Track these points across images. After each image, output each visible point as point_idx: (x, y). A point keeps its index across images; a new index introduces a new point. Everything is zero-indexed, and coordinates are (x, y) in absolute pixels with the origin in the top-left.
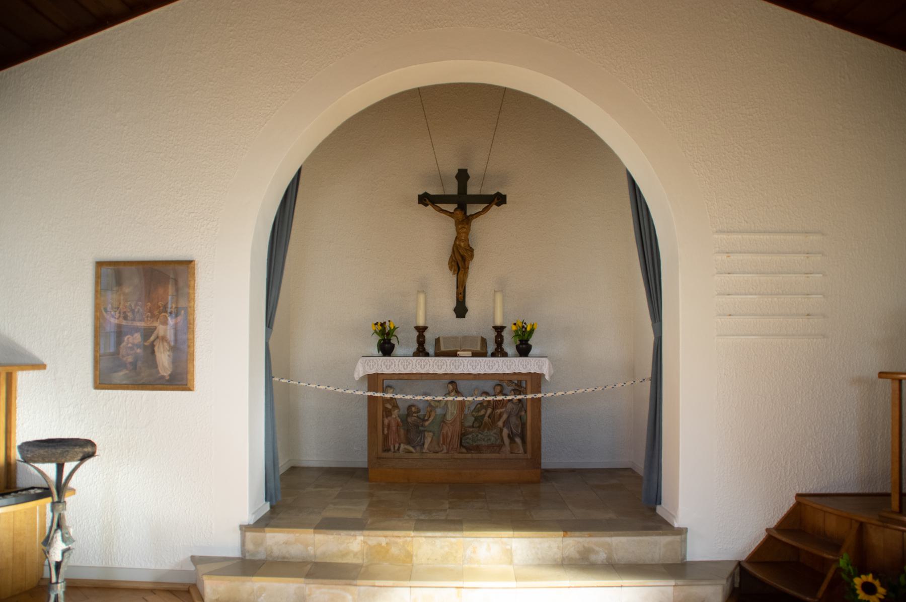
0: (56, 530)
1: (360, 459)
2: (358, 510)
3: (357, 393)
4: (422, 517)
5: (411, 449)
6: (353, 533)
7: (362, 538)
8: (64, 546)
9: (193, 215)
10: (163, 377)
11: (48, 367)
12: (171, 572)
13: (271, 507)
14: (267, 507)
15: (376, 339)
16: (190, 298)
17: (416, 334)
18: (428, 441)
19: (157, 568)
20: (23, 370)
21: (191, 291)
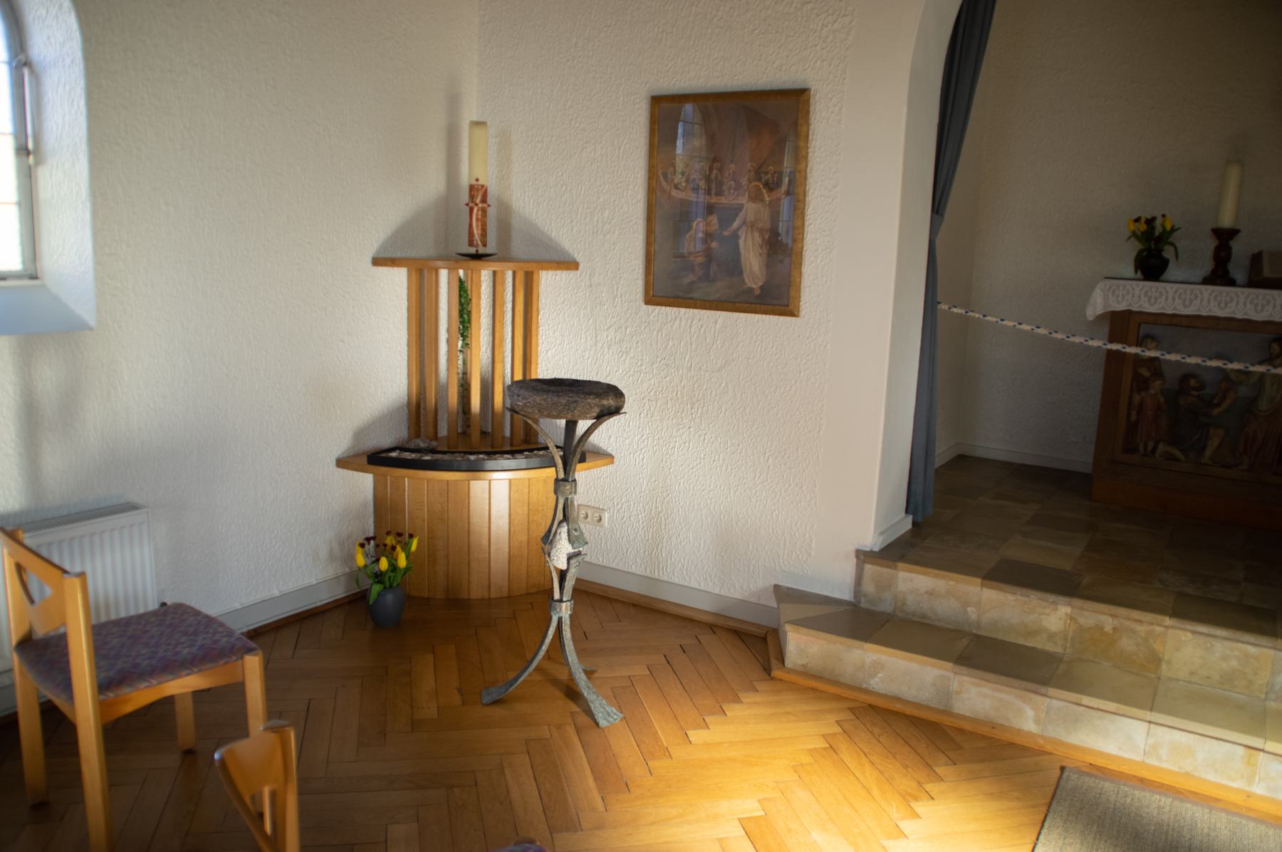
0: (561, 522)
1: (1080, 457)
2: (1064, 555)
3: (1091, 343)
4: (1189, 590)
5: (1181, 456)
6: (1052, 598)
7: (1068, 610)
8: (570, 550)
9: (810, 6)
10: (751, 290)
11: (581, 267)
12: (742, 603)
13: (914, 524)
14: (907, 524)
15: (1134, 247)
16: (800, 156)
17: (1211, 244)
18: (1214, 443)
19: (722, 593)
20: (547, 269)
21: (802, 144)
